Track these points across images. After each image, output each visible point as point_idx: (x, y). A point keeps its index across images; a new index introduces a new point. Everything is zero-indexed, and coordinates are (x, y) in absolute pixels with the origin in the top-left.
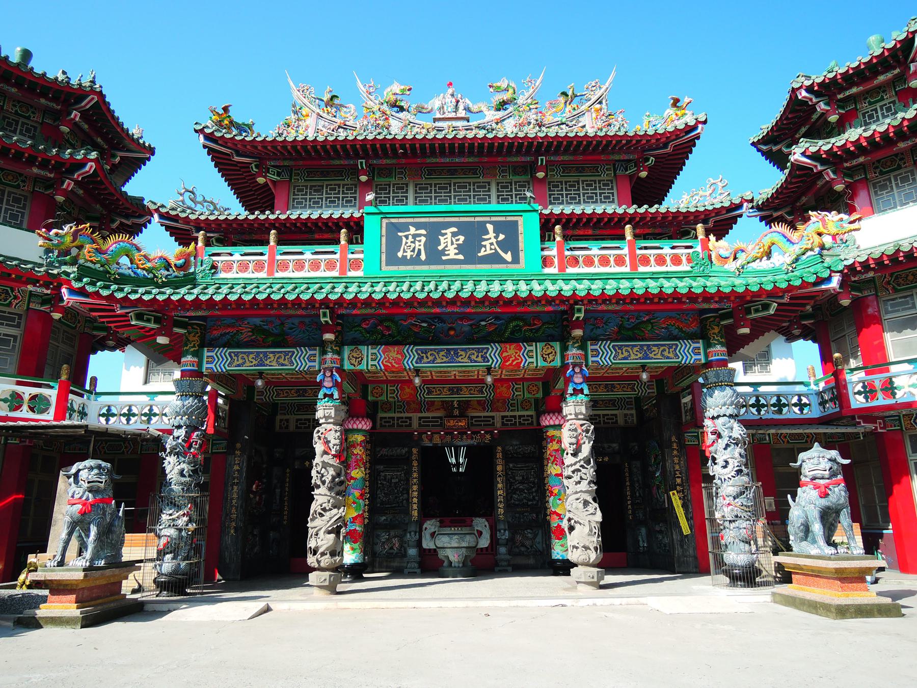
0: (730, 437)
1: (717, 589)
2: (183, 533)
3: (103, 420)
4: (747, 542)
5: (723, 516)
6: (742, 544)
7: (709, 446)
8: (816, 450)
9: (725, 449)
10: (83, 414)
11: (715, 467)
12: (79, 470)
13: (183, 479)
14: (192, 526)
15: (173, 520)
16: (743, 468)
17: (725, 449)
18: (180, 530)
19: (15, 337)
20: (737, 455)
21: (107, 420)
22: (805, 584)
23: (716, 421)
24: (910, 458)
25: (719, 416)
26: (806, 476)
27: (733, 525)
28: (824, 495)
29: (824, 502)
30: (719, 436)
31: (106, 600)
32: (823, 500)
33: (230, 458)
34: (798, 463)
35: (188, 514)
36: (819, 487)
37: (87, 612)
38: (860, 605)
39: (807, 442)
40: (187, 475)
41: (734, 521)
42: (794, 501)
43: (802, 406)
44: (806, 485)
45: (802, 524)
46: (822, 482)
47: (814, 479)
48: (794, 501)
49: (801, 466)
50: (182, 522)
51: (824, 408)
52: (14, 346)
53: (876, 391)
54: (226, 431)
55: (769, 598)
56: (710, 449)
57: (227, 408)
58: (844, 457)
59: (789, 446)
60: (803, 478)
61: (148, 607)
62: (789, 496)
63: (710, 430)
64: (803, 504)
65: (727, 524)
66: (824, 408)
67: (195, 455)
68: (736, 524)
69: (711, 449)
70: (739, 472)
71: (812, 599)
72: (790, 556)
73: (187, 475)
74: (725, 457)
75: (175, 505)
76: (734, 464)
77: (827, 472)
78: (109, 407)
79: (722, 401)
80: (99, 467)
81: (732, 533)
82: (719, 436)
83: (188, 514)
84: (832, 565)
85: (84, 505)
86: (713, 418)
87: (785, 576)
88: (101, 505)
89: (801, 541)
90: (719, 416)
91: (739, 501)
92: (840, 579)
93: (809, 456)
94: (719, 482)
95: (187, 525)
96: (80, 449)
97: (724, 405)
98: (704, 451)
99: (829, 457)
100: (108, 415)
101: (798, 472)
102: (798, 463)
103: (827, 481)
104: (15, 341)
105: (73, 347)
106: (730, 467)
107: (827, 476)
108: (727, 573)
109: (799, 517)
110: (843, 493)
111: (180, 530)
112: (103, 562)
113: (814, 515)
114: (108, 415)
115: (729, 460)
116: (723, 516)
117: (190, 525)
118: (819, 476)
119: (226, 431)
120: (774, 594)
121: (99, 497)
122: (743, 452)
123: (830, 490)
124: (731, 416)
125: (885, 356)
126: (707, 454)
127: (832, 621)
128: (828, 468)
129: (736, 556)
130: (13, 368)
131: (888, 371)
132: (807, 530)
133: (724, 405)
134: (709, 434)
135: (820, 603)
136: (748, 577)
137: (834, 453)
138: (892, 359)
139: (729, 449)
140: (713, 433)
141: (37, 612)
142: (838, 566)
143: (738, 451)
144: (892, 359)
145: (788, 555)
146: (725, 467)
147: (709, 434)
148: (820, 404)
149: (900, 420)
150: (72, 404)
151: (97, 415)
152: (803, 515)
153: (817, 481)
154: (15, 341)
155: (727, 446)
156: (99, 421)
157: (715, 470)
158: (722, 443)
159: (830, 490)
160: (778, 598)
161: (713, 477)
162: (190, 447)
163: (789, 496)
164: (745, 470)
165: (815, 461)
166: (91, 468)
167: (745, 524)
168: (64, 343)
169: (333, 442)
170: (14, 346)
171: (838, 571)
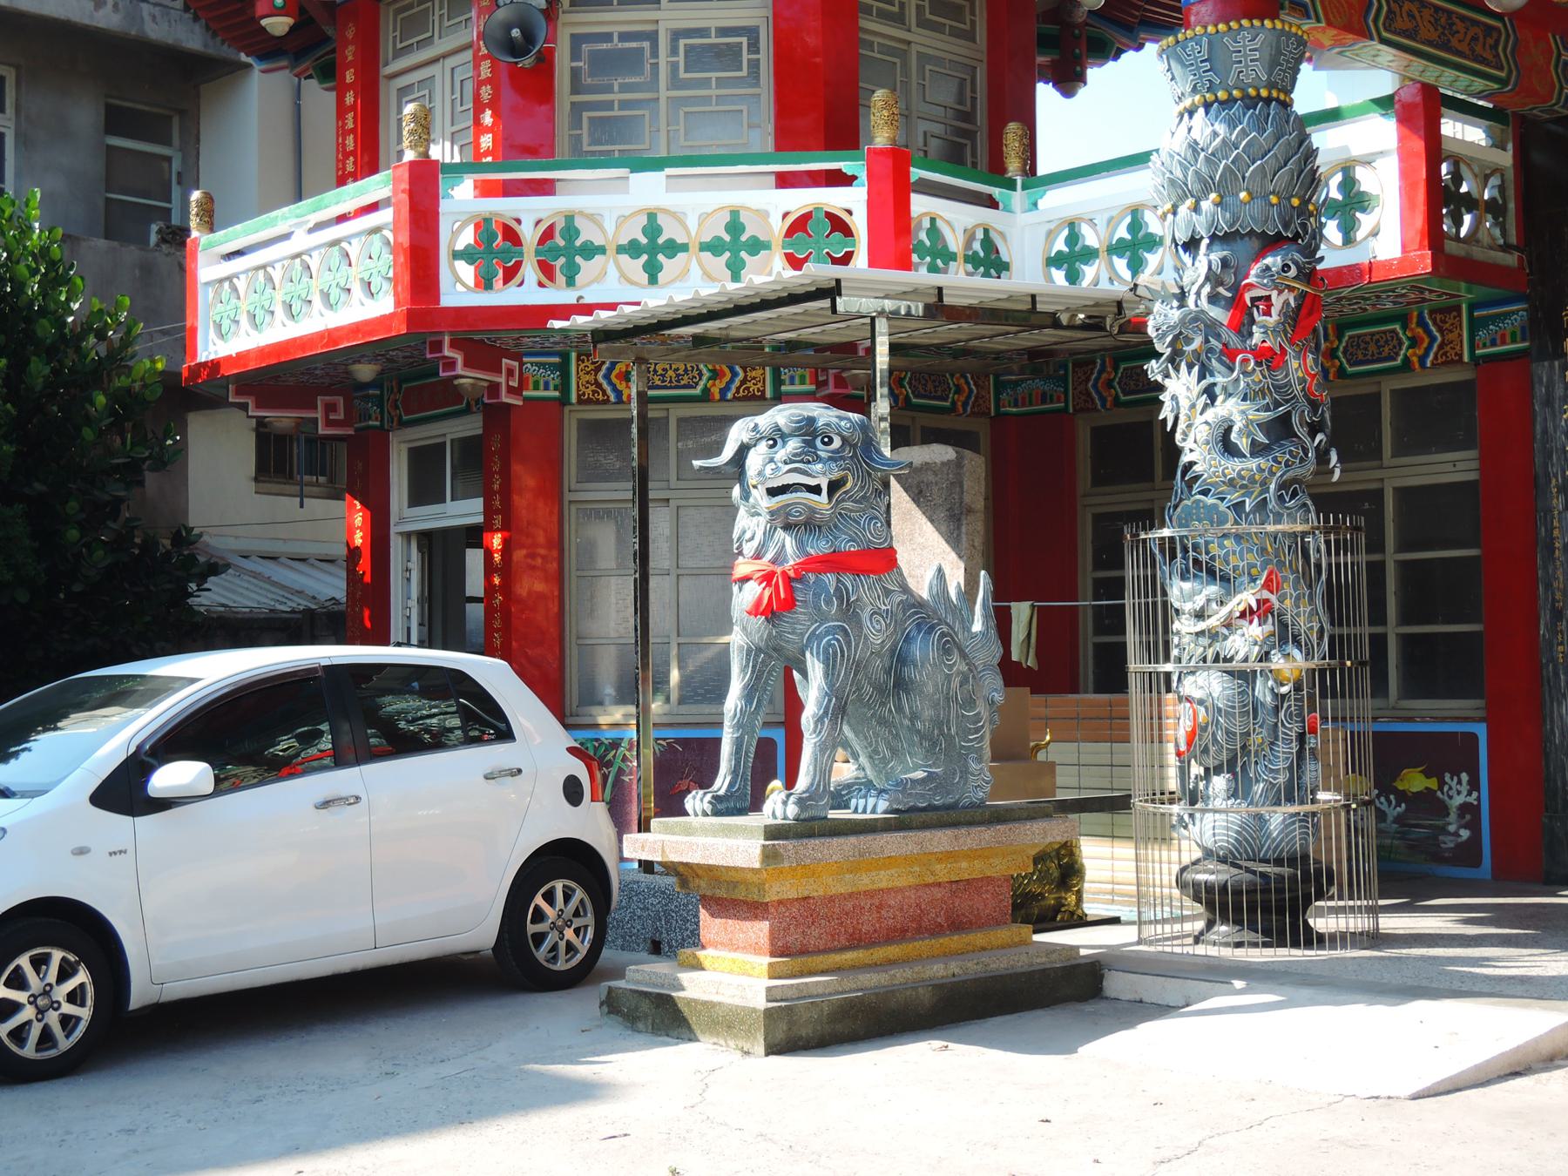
2: (1263, 691)
3: (1059, 276)
10: (990, 260)
12: (743, 450)
13: (1234, 466)
14: (1290, 664)
15: (1213, 636)
18: (1245, 677)
19: (752, 33)
21: (1073, 277)
31: (892, 951)
33: (1542, 371)
35: (1261, 611)
37: (802, 993)
40: (1244, 444)
50: (1245, 641)
52: (754, 65)
54: (1511, 260)
57: (1506, 159)
61: (1116, 984)
67: (1269, 358)
73: (1244, 444)
75: (1211, 573)
78: (1072, 225)
80: (808, 430)
83: (1261, 611)
85: (768, 578)
88: (830, 579)
95: (1265, 657)
96: (1044, 398)
100: (1073, 258)
104: (754, 47)
105: (970, 36)
111: (1245, 677)
112: (883, 805)
114: (1073, 258)
117: (1277, 661)
119: (1511, 260)
121: (819, 547)
130: (763, 136)
141: (685, 977)
150: (933, 230)
151: (1039, 262)
154: (754, 47)
156: (1050, 279)
162: (1243, 322)
166: (776, 437)
168: (923, 23)
170: (754, 65)
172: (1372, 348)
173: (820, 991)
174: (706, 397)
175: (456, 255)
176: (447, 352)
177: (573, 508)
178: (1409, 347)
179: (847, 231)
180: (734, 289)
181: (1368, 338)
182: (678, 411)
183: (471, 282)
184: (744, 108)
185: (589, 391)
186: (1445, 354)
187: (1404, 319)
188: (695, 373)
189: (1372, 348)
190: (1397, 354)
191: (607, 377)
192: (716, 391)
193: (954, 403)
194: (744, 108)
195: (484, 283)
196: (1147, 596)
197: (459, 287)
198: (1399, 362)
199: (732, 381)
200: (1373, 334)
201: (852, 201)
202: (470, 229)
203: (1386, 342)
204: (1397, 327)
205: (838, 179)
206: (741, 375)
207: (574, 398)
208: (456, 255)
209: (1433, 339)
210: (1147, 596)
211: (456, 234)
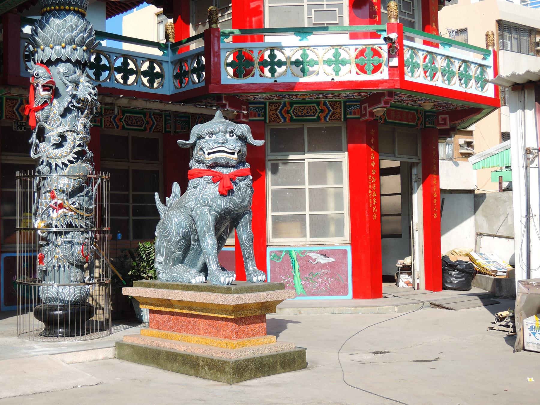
0: (74, 96)
1: (28, 342)
4: (77, 266)
5: (50, 225)
6: (73, 269)
7: (37, 110)
8: (218, 123)
9: (63, 116)
11: (42, 145)
16: (87, 149)
17: (63, 116)
20: (80, 128)
22: (172, 329)
23: (52, 69)
24: (268, 158)
25: (59, 61)
26: (200, 162)
27: (60, 240)
28: (226, 192)
29: (224, 203)
30: (56, 94)
32: (224, 199)
34: (191, 141)
36: (220, 180)
38: (262, 358)
39: (145, 129)
41: (66, 233)
42: (164, 202)
43: (150, 74)
44: (199, 174)
45: (183, 237)
46: (225, 171)
47: (216, 164)
48: (164, 202)
49: (194, 145)
51: (181, 82)
53: (253, 65)
55: (110, 352)
56: (37, 114)
58: (256, 137)
59: (123, 133)
60: (193, 165)
62: (157, 195)
63: (42, 82)
64: (192, 204)
65: (52, 237)
66: (181, 82)
68: (69, 237)
69: (40, 114)
70: (80, 155)
71: (189, 352)
72: (155, 286)
74: (60, 130)
76: (73, 141)
77: (235, 156)
79: (68, 36)
81: (60, 252)
82: (56, 94)
84: (232, 300)
86: (49, 63)
87: (126, 312)
89: (174, 264)
90: (59, 61)
91: (80, 200)
92: (238, 321)
93: (211, 129)
94: (44, 169)
97: (71, 42)
98: (28, 117)
99: (239, 133)
101: (187, 153)
102: (191, 141)
103: (232, 170)
106: (68, 146)
107: (234, 163)
108: (39, 315)
109: (180, 225)
110: (249, 191)
113: (206, 220)
115: (69, 136)
116: (50, 225)
118: (223, 161)
120: (119, 345)
122: (88, 122)
123: (236, 184)
124: (78, 64)
125: (261, 22)
126: (31, 123)
127: (227, 387)
128: (237, 149)
129: (60, 288)
131: (261, 40)
132: (189, 245)
133: (71, 42)
134: (40, 89)
135: (203, 359)
136: (73, 321)
137: (243, 129)
138: (267, 26)
139: (69, 117)
140: (45, 88)
142: (240, 302)
143: (81, 122)
144: (267, 26)
145: (150, 286)
146: (59, 145)
147: (40, 89)
148: (175, 77)
149: (265, 108)
152: (186, 223)
153: (219, 169)
155: (67, 111)
157: (45, 150)
158: (58, 106)
159: (236, 184)
160: (127, 351)
161: (37, 162)
163: (157, 195)
164: (90, 154)
165: (220, 137)
167: (79, 238)
169: (197, 340)
171: (238, 308)
172: (305, 111)
173: (202, 323)
174: (319, 119)
175: (228, 65)
176: (224, 102)
177: (270, 162)
178: (319, 113)
179: (380, 56)
180: (492, 68)
181: (303, 108)
182: (307, 125)
183: (232, 74)
184: (337, 9)
185: (273, 117)
186: (335, 116)
187: (318, 104)
188: (314, 110)
189: (134, 121)
190: (315, 115)
191: (280, 112)
192: (322, 117)
193: (417, 124)
194: (337, 9)
195: (236, 75)
196: (27, 188)
197: (229, 77)
198: (315, 117)
199: (328, 113)
200: (134, 117)
201: (380, 43)
202: (232, 56)
203: (311, 110)
204: (295, 118)
205: (374, 35)
206: (278, 112)
207: (268, 121)
208: (228, 65)
209: (330, 111)
210: (27, 188)
211: (227, 57)
